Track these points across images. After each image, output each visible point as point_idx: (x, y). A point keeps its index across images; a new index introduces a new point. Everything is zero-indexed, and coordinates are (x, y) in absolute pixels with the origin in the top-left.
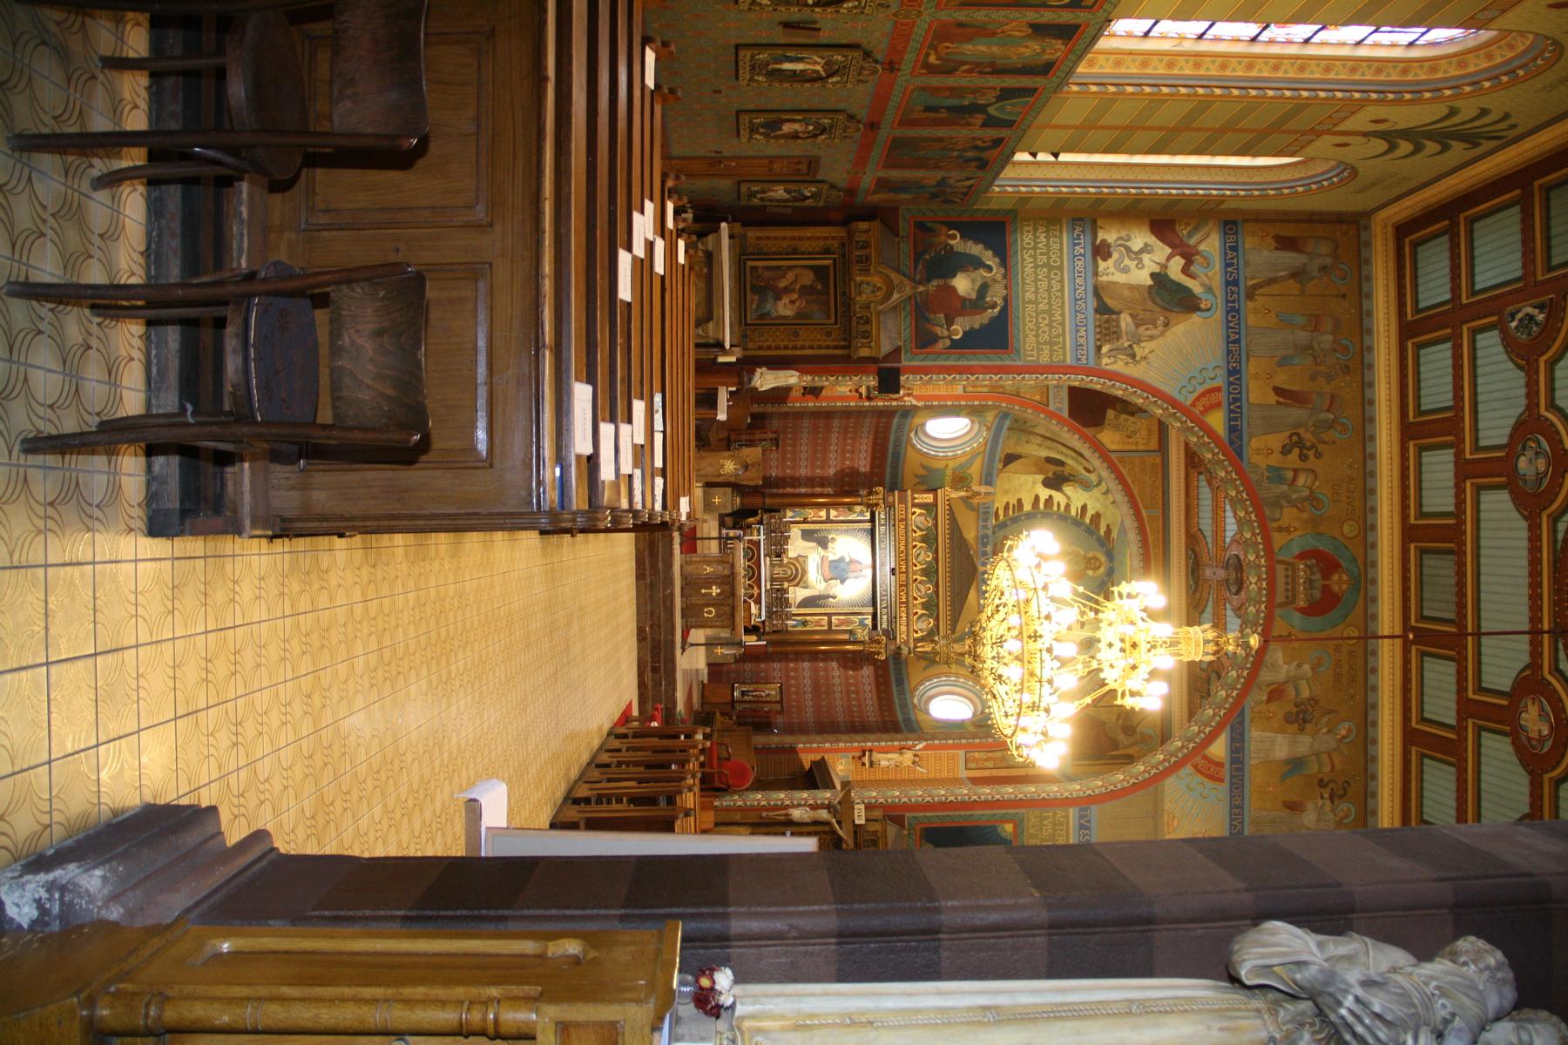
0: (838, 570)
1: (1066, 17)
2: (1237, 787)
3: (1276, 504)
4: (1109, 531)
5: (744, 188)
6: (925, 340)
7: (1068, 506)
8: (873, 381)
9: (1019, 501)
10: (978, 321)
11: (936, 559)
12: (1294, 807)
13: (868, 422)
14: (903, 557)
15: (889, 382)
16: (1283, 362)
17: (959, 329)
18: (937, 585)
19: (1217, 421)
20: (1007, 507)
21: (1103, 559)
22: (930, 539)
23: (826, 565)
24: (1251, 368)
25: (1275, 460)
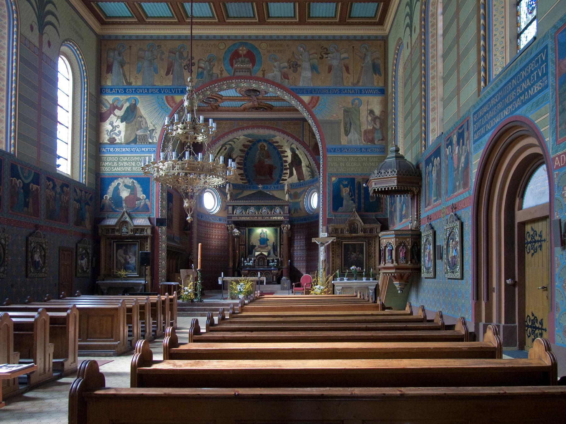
2: (321, 91)
4: (249, 141)
7: (241, 157)
9: (239, 175)
10: (139, 189)
11: (253, 206)
18: (263, 206)
20: (242, 179)
21: (260, 144)
23: (262, 246)
24: (158, 84)
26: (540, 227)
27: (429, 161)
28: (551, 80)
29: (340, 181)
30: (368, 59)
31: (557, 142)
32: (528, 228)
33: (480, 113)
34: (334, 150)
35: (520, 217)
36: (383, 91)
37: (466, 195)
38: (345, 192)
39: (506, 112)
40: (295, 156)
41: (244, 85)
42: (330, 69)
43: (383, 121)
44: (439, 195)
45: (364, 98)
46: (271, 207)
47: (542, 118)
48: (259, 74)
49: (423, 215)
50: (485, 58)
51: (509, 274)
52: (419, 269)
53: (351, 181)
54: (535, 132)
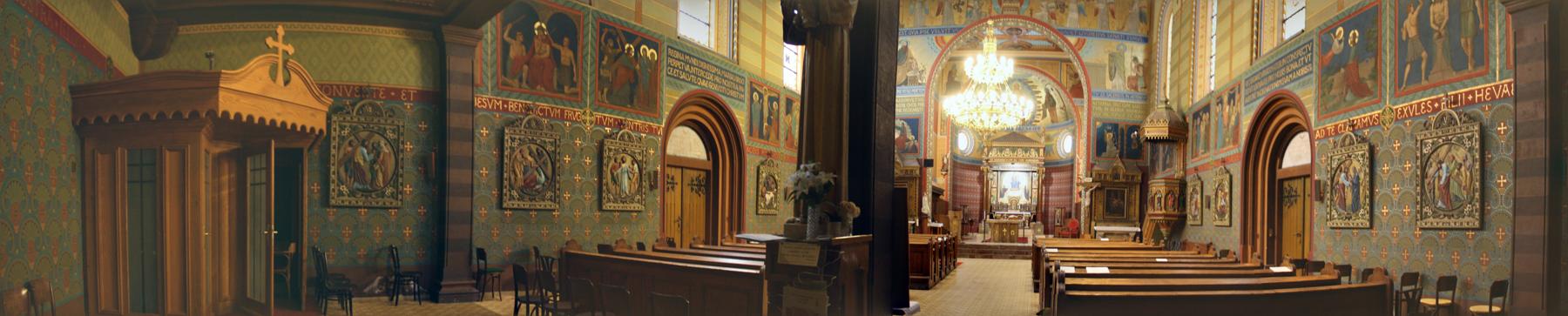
0: (1016, 185)
1: (783, 103)
2: (1088, 34)
3: (980, 14)
5: (1362, 219)
6: (915, 150)
8: (930, 170)
10: (908, 130)
12: (1097, 12)
13: (959, 171)
14: (1007, 160)
15: (929, 163)
16: (927, 12)
17: (911, 137)
19: (948, 37)
22: (1001, 149)
24: (929, 25)
25: (963, 14)
26: (1297, 184)
27: (1196, 115)
28: (1315, 68)
29: (1104, 125)
30: (1136, 7)
31: (1319, 118)
32: (1286, 184)
33: (1252, 80)
34: (1099, 95)
35: (1279, 175)
36: (1146, 40)
37: (1235, 151)
38: (1109, 136)
39: (1276, 85)
40: (1049, 96)
41: (1011, 24)
42: (1097, 12)
43: (1148, 70)
44: (1207, 148)
45: (1129, 44)
46: (1026, 150)
47: (1307, 95)
48: (1027, 14)
49: (1190, 166)
50: (1256, 34)
51: (1271, 225)
52: (1185, 217)
53: (1115, 126)
54: (1300, 106)
